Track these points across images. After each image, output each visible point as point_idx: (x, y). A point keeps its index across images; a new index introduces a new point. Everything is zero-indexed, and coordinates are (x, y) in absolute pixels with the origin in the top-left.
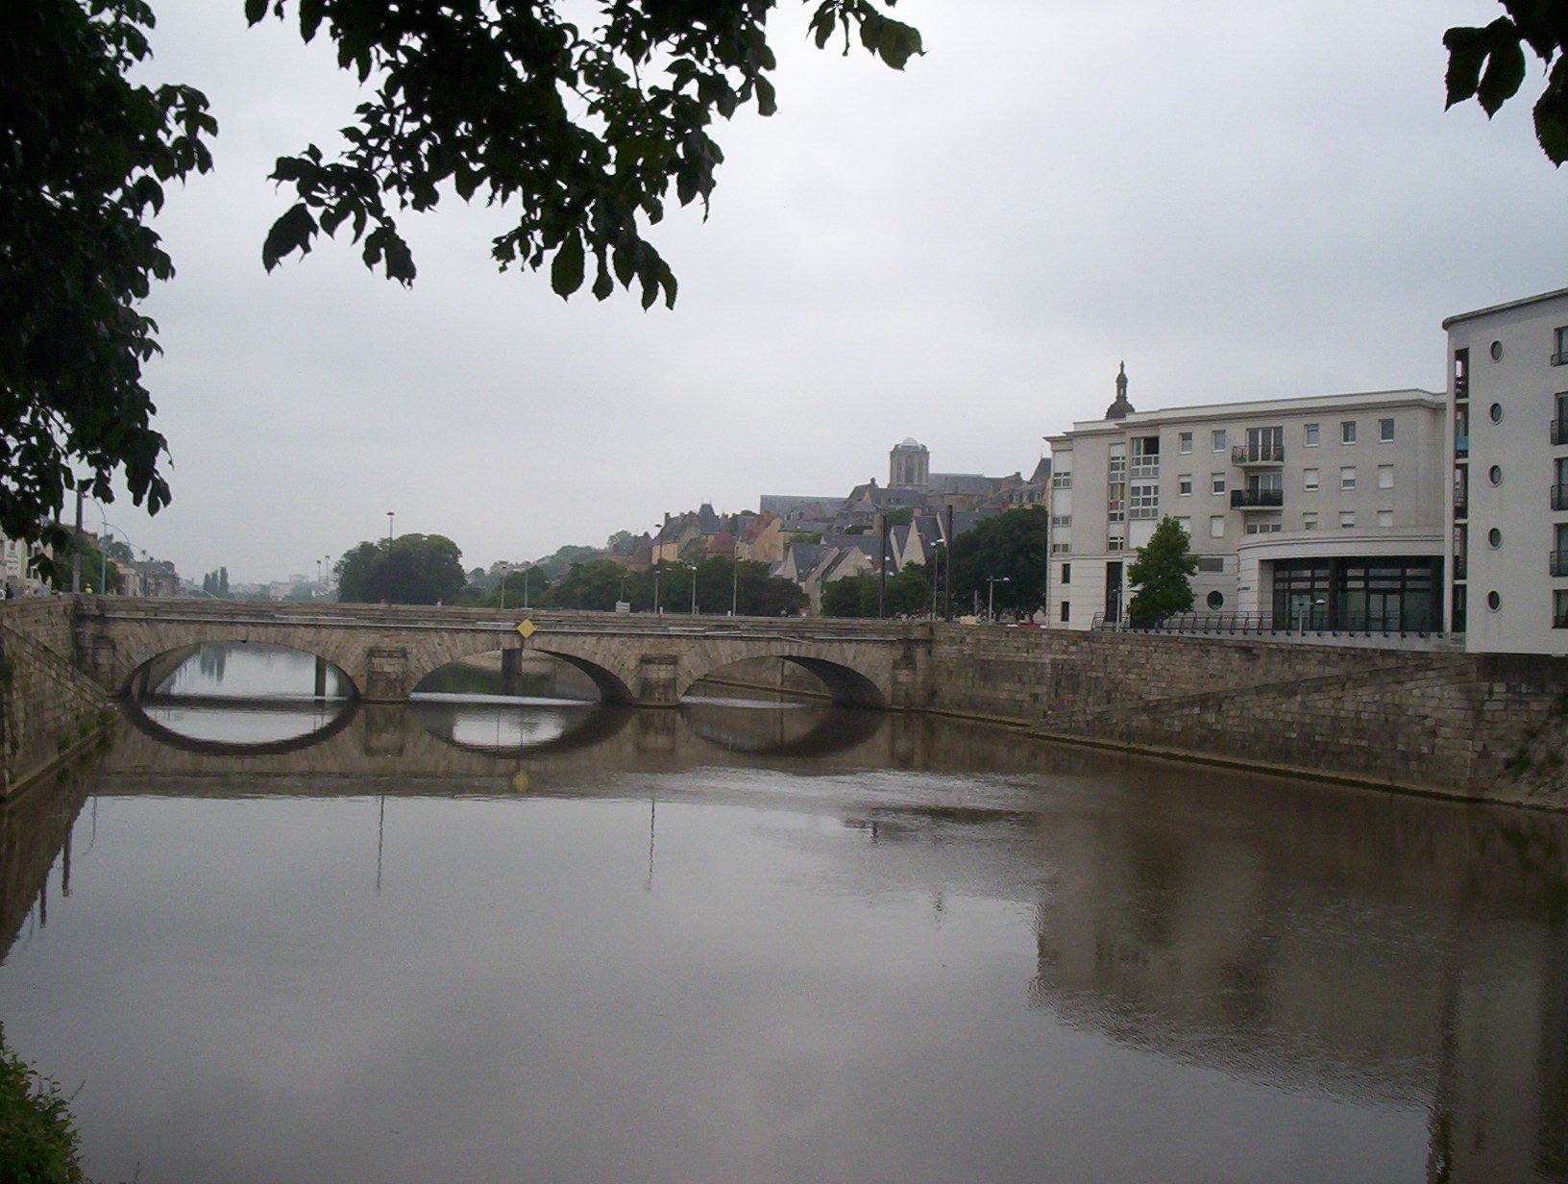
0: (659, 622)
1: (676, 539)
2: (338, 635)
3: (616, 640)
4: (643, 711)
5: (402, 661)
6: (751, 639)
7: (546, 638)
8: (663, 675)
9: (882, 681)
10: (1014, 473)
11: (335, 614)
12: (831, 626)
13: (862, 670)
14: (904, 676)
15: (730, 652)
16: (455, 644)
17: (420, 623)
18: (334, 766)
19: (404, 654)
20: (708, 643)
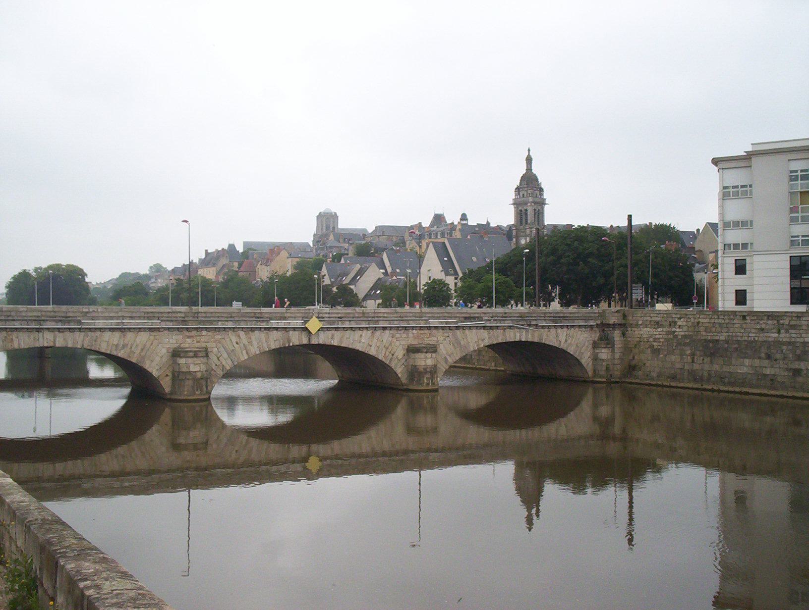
0: (420, 316)
1: (214, 265)
2: (143, 337)
3: (387, 332)
4: (411, 394)
5: (205, 360)
6: (491, 328)
7: (329, 333)
8: (430, 362)
9: (586, 359)
10: (418, 223)
11: (139, 318)
12: (549, 315)
13: (571, 350)
14: (604, 354)
15: (476, 340)
16: (250, 343)
17: (506, 322)
18: (142, 464)
19: (206, 353)
20: (459, 333)
